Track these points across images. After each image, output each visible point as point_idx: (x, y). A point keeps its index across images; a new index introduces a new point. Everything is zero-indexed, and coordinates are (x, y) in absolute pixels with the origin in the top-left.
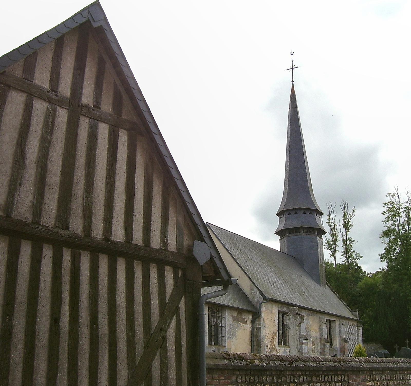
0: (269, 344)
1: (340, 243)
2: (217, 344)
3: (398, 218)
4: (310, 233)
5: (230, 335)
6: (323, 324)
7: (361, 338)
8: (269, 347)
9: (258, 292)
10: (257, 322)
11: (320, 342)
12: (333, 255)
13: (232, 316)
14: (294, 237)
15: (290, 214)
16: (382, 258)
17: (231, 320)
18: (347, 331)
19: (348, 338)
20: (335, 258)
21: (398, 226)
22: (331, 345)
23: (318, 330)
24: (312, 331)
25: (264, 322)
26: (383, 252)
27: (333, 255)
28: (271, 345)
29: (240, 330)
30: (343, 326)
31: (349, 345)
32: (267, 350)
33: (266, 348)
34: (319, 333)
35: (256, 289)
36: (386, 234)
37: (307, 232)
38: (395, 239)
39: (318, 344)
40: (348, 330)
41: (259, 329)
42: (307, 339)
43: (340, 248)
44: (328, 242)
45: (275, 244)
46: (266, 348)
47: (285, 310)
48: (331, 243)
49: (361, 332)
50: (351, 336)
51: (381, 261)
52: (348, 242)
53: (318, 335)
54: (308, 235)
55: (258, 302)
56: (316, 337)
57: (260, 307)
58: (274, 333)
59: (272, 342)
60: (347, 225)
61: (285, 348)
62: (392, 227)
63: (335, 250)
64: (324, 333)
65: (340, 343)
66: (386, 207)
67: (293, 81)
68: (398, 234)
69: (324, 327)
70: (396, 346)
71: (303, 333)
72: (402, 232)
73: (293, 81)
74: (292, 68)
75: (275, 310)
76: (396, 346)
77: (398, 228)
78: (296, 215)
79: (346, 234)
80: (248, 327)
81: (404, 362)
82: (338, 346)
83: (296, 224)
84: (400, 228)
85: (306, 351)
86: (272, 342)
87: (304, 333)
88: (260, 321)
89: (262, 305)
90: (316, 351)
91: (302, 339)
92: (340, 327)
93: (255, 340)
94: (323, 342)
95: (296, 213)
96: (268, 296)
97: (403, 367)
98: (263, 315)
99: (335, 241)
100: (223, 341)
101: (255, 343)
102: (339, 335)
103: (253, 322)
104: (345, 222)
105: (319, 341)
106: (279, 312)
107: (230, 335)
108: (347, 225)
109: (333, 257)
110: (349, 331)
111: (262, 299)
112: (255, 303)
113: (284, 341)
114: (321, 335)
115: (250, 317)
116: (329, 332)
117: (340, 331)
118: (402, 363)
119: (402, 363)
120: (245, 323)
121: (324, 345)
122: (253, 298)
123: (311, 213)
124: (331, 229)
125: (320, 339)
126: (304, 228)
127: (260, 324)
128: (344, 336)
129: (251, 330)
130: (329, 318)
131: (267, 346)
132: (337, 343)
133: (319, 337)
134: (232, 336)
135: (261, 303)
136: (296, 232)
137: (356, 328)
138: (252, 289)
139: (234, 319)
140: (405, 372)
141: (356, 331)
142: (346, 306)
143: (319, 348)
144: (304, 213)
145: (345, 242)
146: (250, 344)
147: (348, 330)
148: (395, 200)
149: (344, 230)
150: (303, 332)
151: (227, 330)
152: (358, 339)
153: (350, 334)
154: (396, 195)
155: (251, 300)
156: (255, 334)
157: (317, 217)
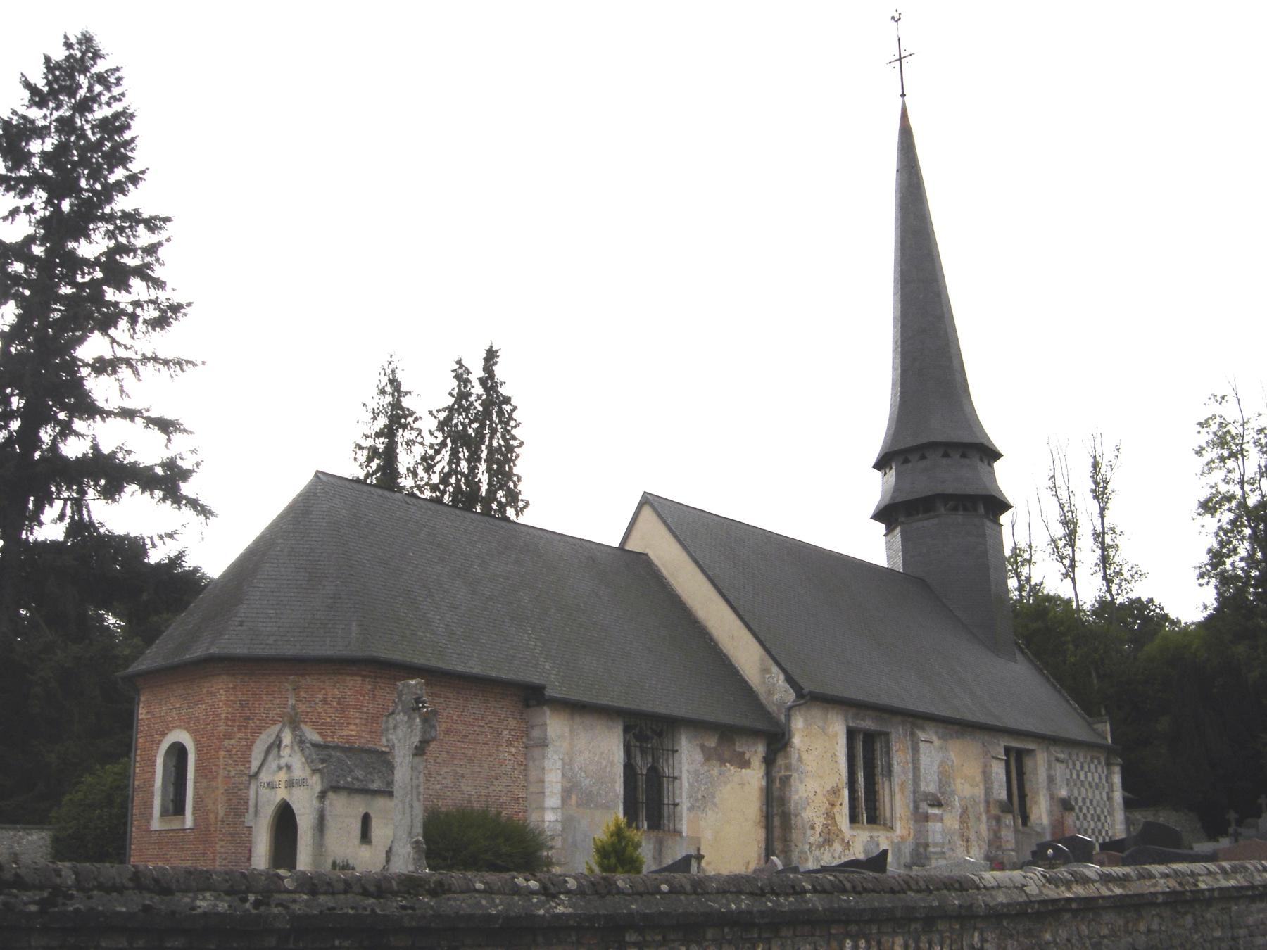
0: (819, 821)
1: (1085, 542)
2: (873, 819)
3: (1240, 461)
4: (965, 509)
5: (697, 800)
6: (994, 763)
7: (1118, 795)
8: (818, 830)
9: (782, 677)
10: (780, 761)
11: (988, 811)
12: (1070, 572)
13: (702, 747)
14: (926, 524)
15: (906, 461)
16: (1202, 576)
17: (699, 757)
18: (1075, 776)
19: (1076, 799)
20: (1074, 583)
21: (1242, 483)
22: (1025, 818)
23: (979, 778)
24: (959, 781)
25: (800, 759)
26: (1206, 558)
27: (1070, 572)
28: (825, 826)
29: (729, 787)
30: (1058, 764)
31: (1081, 816)
32: (812, 840)
33: (809, 832)
34: (982, 786)
35: (775, 669)
36: (1208, 507)
37: (955, 509)
38: (1233, 522)
39: (978, 819)
40: (1078, 776)
41: (786, 781)
42: (939, 805)
43: (1087, 552)
44: (1054, 541)
45: (872, 546)
46: (809, 832)
47: (868, 724)
48: (1061, 544)
49: (1117, 779)
50: (1087, 792)
51: (1201, 585)
52: (1108, 539)
53: (979, 792)
54: (959, 517)
55: (781, 704)
56: (973, 798)
57: (788, 717)
58: (835, 791)
59: (829, 815)
60: (1101, 493)
61: (870, 830)
62: (1223, 488)
63: (1073, 560)
64: (996, 785)
65: (1051, 812)
66: (1204, 431)
67: (903, 95)
68: (1242, 505)
69: (998, 770)
70: (1232, 816)
71: (929, 785)
72: (1252, 501)
73: (903, 95)
74: (900, 59)
75: (837, 728)
76: (1232, 816)
77: (1242, 488)
78: (923, 464)
79: (1102, 516)
80: (754, 776)
81: (828, 887)
82: (1046, 821)
83: (923, 486)
84: (1247, 488)
85: (938, 838)
86: (829, 815)
87: (932, 788)
88: (787, 756)
89: (792, 712)
90: (973, 836)
91: (924, 807)
92: (1050, 768)
93: (777, 814)
94: (995, 811)
95: (923, 457)
96: (808, 687)
97: (812, 911)
98: (796, 740)
99: (1071, 536)
100: (674, 817)
101: (777, 821)
102: (1049, 788)
103: (769, 761)
104: (1097, 484)
105: (982, 808)
106: (851, 734)
107: (697, 800)
108: (1101, 493)
109: (1068, 580)
110: (1082, 777)
111: (791, 696)
112: (775, 708)
113: (867, 808)
114: (988, 791)
115: (761, 749)
116: (1015, 782)
117: (1051, 779)
118: (815, 890)
119: (820, 892)
120: (745, 764)
121: (998, 819)
122: (770, 693)
123: (964, 456)
124: (1062, 506)
125: (987, 802)
126: (945, 498)
127: (788, 767)
128: (1063, 793)
129: (764, 783)
130: (1015, 744)
131: (813, 828)
132: (1041, 812)
133: (983, 797)
134: (703, 802)
135: (790, 708)
136: (927, 511)
137: (1102, 769)
138: (765, 670)
139: (709, 755)
140: (833, 931)
141: (1103, 776)
142: (1075, 709)
143: (983, 828)
144: (946, 455)
145: (1099, 537)
146: (763, 824)
147: (1078, 776)
148: (1230, 412)
149: (1094, 506)
150: (927, 786)
151: (686, 785)
152: (1110, 798)
153: (1083, 786)
154: (1231, 398)
155: (764, 701)
156: (776, 794)
157: (982, 467)
